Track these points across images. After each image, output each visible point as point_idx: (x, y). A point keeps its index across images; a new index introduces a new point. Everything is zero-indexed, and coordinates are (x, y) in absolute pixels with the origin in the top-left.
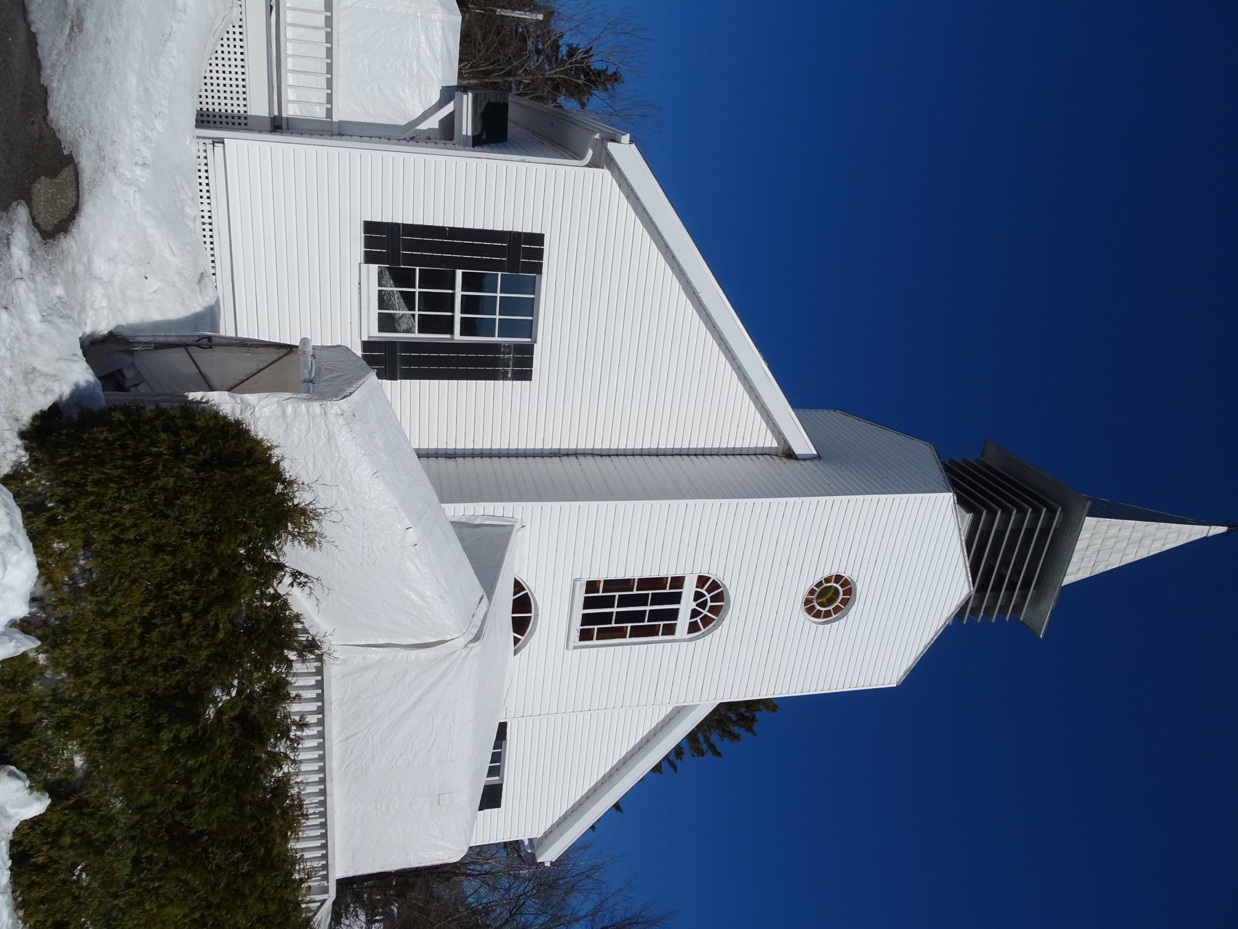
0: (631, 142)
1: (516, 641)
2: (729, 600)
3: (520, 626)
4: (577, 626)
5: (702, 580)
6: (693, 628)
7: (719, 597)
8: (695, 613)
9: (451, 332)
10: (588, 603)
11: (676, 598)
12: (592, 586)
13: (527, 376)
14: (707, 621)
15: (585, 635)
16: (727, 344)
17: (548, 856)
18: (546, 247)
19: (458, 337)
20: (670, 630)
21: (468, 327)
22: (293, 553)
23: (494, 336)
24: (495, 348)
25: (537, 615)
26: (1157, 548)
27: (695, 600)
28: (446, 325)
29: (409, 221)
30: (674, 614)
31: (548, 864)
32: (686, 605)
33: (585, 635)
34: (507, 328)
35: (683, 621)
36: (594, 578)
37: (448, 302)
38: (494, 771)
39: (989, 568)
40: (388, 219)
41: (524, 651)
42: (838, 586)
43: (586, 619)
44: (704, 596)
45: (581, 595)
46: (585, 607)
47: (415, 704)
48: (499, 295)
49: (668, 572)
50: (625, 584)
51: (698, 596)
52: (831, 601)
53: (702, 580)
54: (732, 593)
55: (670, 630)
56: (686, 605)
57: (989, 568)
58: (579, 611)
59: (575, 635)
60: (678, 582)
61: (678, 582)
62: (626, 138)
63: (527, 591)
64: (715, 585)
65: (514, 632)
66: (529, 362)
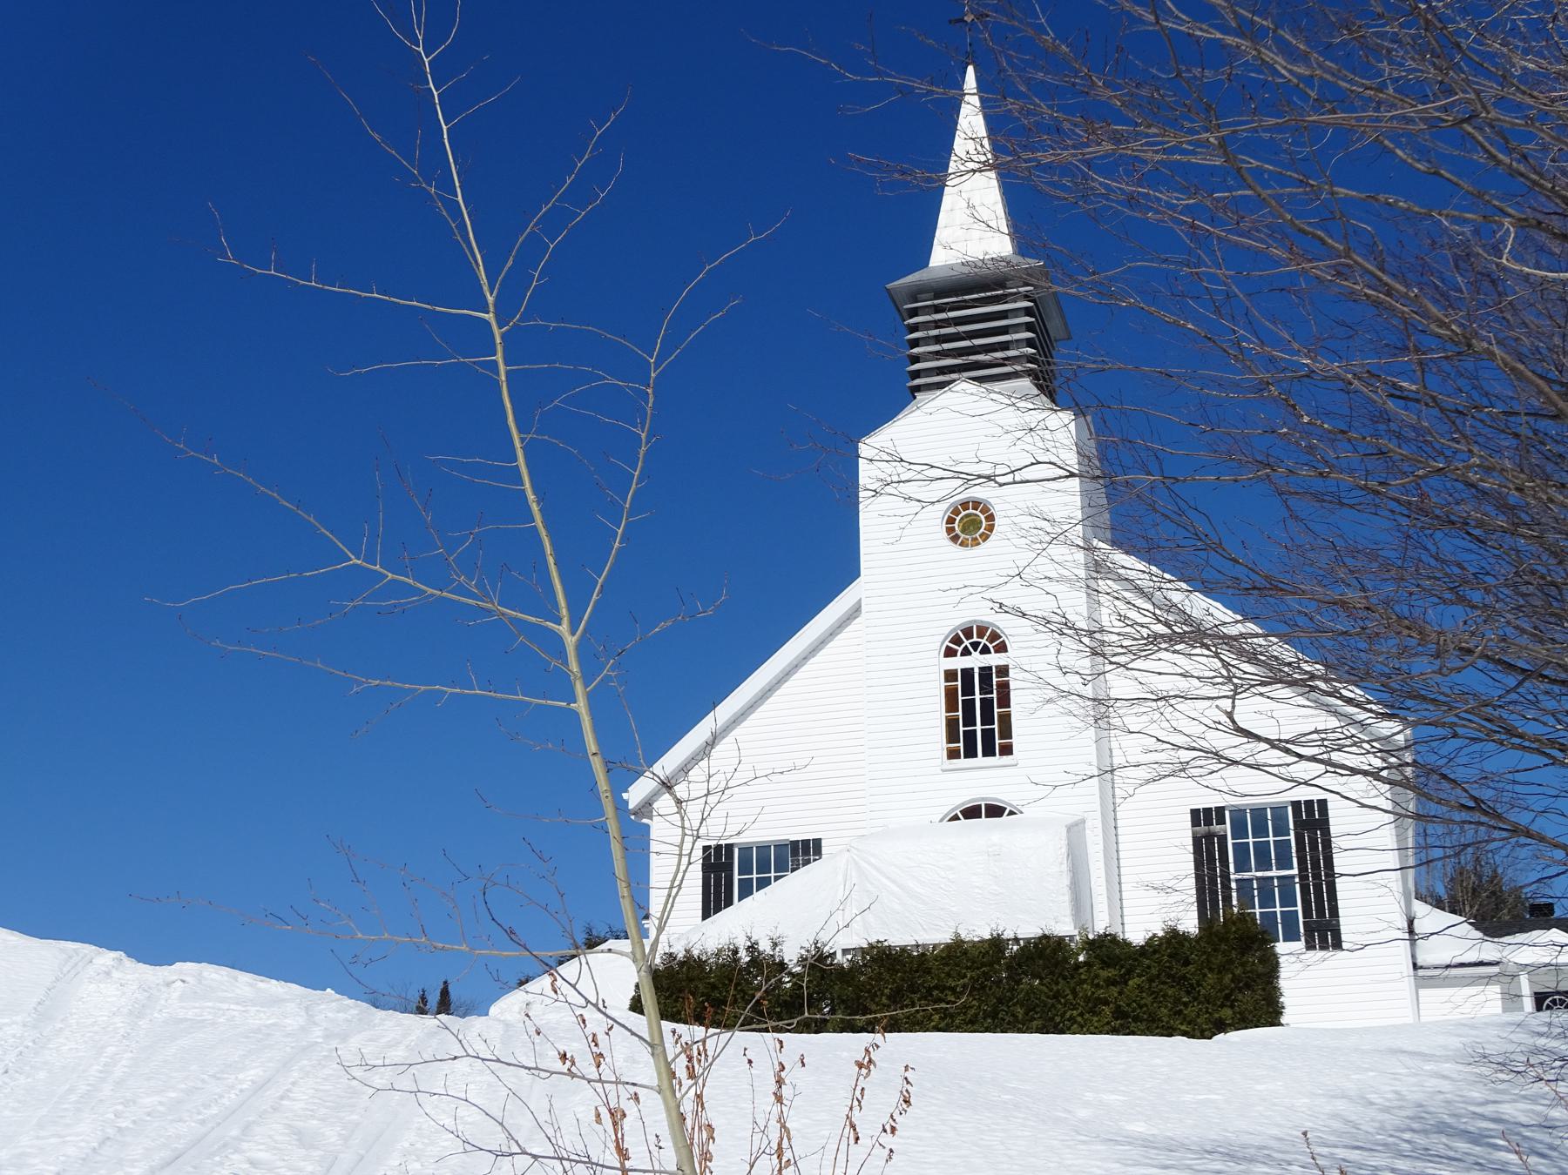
0: (626, 791)
1: (1012, 813)
2: (970, 622)
3: (995, 811)
4: (997, 760)
5: (950, 653)
6: (1002, 648)
7: (968, 632)
8: (985, 651)
9: (1293, 877)
10: (971, 752)
11: (967, 674)
12: (953, 754)
14: (995, 636)
15: (1007, 750)
16: (788, 669)
18: (1201, 807)
20: (1003, 671)
23: (1296, 911)
25: (983, 799)
27: (970, 654)
30: (986, 672)
32: (976, 661)
33: (1007, 750)
34: (1281, 829)
35: (994, 660)
36: (945, 753)
38: (956, 818)
39: (941, 371)
42: (958, 519)
43: (989, 751)
44: (980, 643)
45: (963, 762)
47: (894, 882)
48: (755, 876)
50: (952, 725)
51: (966, 652)
52: (978, 524)
54: (958, 622)
55: (1003, 671)
56: (976, 661)
57: (941, 371)
58: (980, 760)
59: (1006, 759)
60: (950, 675)
61: (950, 675)
62: (625, 796)
64: (957, 640)
65: (1001, 816)
66: (806, 843)
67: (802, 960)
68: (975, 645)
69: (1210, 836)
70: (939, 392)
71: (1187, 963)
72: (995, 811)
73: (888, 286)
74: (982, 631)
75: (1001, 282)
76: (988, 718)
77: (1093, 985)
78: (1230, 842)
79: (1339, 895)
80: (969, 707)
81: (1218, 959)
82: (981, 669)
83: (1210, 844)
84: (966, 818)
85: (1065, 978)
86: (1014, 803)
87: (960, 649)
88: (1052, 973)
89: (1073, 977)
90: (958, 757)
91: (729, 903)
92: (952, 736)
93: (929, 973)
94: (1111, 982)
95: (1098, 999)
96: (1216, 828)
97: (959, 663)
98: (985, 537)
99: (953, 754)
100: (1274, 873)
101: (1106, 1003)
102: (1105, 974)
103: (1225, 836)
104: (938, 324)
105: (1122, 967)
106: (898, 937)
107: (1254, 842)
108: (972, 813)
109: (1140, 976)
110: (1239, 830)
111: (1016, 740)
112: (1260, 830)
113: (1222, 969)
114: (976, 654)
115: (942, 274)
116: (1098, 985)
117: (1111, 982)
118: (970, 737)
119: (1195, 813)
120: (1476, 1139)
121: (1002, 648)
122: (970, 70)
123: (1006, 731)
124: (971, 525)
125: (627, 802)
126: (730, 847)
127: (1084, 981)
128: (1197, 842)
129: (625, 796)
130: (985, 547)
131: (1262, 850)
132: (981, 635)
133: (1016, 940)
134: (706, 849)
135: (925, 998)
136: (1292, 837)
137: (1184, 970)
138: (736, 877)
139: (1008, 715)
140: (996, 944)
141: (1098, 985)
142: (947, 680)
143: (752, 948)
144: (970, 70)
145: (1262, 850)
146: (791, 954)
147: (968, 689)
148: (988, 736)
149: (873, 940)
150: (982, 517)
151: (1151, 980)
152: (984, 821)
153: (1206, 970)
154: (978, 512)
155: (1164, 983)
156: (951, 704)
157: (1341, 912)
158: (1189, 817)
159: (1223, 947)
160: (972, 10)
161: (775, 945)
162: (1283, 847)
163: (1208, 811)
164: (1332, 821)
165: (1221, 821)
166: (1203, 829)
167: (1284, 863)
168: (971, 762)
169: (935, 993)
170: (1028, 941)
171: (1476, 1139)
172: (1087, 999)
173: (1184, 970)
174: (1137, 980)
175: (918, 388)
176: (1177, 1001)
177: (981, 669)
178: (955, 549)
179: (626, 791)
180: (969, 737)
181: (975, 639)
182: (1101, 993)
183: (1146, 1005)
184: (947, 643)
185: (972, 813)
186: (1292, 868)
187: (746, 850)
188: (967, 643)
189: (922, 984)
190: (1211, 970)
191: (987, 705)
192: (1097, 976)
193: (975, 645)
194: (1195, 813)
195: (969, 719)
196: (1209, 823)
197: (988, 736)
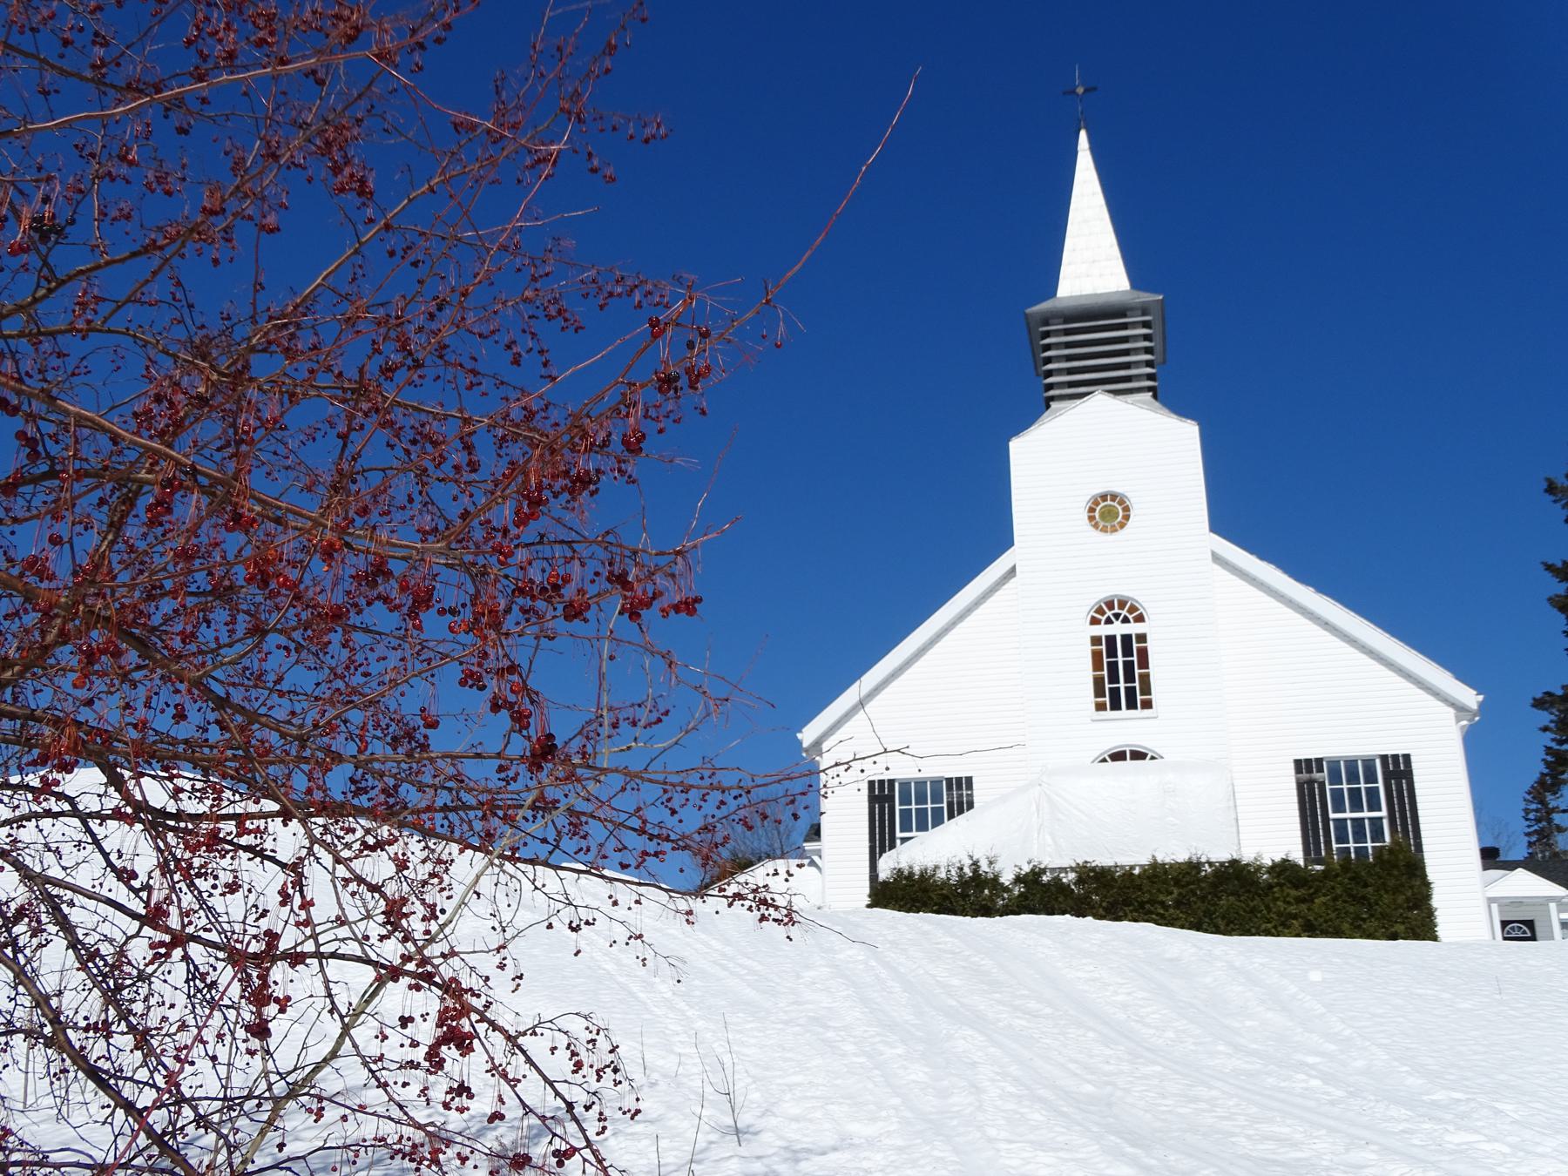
3: (1138, 755)
4: (1139, 712)
5: (1094, 621)
6: (1140, 619)
7: (1110, 605)
8: (1126, 620)
9: (1381, 818)
10: (1116, 706)
11: (1111, 640)
12: (1100, 707)
13: (1303, 766)
14: (1133, 609)
15: (1147, 705)
17: (1470, 698)
19: (1384, 813)
20: (1142, 638)
21: (1373, 805)
22: (942, 875)
26: (1099, 200)
28: (1376, 823)
30: (1127, 639)
31: (1481, 698)
32: (1118, 629)
33: (1147, 705)
34: (1370, 777)
35: (1133, 629)
36: (1093, 706)
37: (1358, 823)
38: (1104, 760)
43: (1132, 705)
45: (1109, 714)
46: (1136, 708)
49: (1088, 649)
50: (1098, 683)
51: (1109, 621)
54: (1093, 602)
55: (1142, 638)
58: (1124, 712)
59: (1147, 712)
60: (1096, 640)
61: (1096, 640)
62: (799, 736)
63: (1128, 750)
64: (1100, 611)
67: (1018, 880)
68: (1117, 616)
69: (1311, 782)
70: (1078, 402)
71: (1366, 885)
72: (1138, 755)
73: (1029, 311)
74: (1122, 604)
76: (1129, 677)
77: (1285, 902)
78: (1328, 787)
79: (1423, 834)
80: (1113, 667)
81: (1392, 882)
85: (1259, 896)
86: (1157, 750)
87: (1103, 619)
88: (1249, 891)
89: (1267, 895)
90: (1105, 709)
91: (942, 822)
92: (1099, 691)
93: (1140, 889)
94: (1299, 900)
95: (1290, 914)
96: (1316, 775)
97: (1103, 630)
98: (1122, 526)
99: (1100, 707)
100: (1348, 815)
101: (1295, 917)
102: (1294, 893)
103: (1323, 783)
104: (1068, 345)
105: (1310, 887)
106: (1103, 858)
107: (1349, 789)
108: (1118, 756)
109: (1325, 895)
110: (1335, 777)
111: (1155, 696)
112: (921, 799)
113: (1396, 891)
114: (1117, 624)
115: (1072, 303)
116: (1289, 903)
117: (1299, 900)
118: (1115, 693)
119: (1298, 763)
122: (1083, 135)
124: (1109, 514)
125: (800, 743)
126: (891, 782)
127: (1277, 899)
128: (1300, 786)
129: (799, 736)
130: (1121, 534)
131: (1354, 794)
132: (1103, 613)
133: (1211, 864)
135: (1136, 911)
137: (1363, 891)
138: (898, 808)
139: (1147, 675)
140: (1193, 867)
141: (1289, 903)
142: (1093, 644)
143: (975, 864)
144: (1083, 135)
145: (1354, 794)
146: (917, 870)
147: (1112, 652)
148: (1131, 693)
149: (1080, 862)
150: (1120, 508)
151: (1335, 899)
152: (1129, 764)
153: (1382, 892)
154: (1115, 504)
155: (1345, 902)
156: (1097, 665)
157: (1425, 848)
158: (1292, 766)
159: (1396, 873)
160: (1082, 84)
161: (991, 863)
162: (1372, 794)
163: (1308, 761)
164: (1415, 772)
165: (1320, 770)
166: (1305, 776)
168: (1116, 714)
169: (1147, 906)
170: (1222, 864)
172: (1280, 914)
173: (1363, 891)
174: (1323, 899)
175: (1052, 398)
176: (1358, 917)
179: (800, 731)
180: (1115, 693)
181: (1116, 610)
182: (1293, 909)
183: (1331, 920)
184: (1092, 613)
185: (1118, 756)
186: (1380, 809)
187: (905, 785)
188: (1109, 613)
189: (1135, 899)
190: (1387, 892)
191: (1129, 667)
192: (1288, 895)
193: (1117, 616)
194: (1298, 763)
195: (1114, 678)
196: (1310, 771)
197: (1131, 693)
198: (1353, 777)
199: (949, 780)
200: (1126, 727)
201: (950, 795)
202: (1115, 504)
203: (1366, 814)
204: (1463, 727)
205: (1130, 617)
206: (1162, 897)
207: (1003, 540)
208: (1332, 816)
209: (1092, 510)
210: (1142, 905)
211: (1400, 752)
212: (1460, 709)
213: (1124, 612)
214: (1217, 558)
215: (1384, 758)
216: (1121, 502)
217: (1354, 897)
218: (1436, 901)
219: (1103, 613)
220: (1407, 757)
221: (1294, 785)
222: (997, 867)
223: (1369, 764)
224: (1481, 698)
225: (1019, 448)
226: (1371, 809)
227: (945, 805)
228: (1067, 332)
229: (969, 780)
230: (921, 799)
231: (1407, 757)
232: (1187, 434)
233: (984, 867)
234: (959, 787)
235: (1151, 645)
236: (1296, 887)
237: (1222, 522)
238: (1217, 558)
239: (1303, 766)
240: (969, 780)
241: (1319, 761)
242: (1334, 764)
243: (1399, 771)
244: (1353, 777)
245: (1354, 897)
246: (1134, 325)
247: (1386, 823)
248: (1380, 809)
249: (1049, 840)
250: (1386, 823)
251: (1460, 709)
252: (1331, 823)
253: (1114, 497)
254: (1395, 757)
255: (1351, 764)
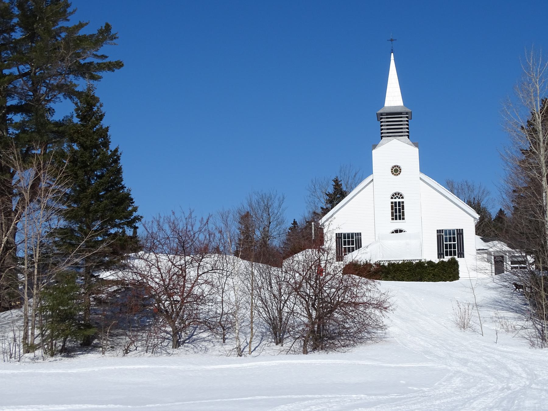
1: (404, 232)
3: (401, 231)
4: (401, 221)
5: (392, 198)
6: (403, 198)
7: (396, 194)
8: (399, 198)
10: (396, 219)
11: (396, 203)
12: (393, 219)
13: (439, 231)
14: (401, 195)
15: (403, 219)
17: (478, 216)
18: (439, 229)
20: (403, 202)
21: (454, 241)
24: (356, 239)
28: (454, 245)
29: (437, 252)
30: (399, 202)
31: (479, 216)
32: (397, 200)
33: (403, 219)
34: (454, 234)
35: (401, 200)
38: (393, 232)
40: (437, 255)
41: (406, 230)
43: (400, 219)
45: (395, 221)
48: (452, 236)
50: (392, 213)
51: (395, 198)
53: (392, 198)
55: (403, 202)
58: (398, 221)
60: (392, 203)
61: (392, 203)
64: (393, 195)
67: (375, 264)
68: (397, 197)
69: (440, 235)
71: (445, 267)
72: (401, 231)
74: (399, 194)
75: (401, 113)
78: (444, 236)
81: (450, 266)
82: (398, 202)
83: (440, 237)
84: (396, 233)
87: (394, 197)
91: (354, 251)
94: (432, 270)
96: (441, 234)
97: (394, 200)
99: (393, 219)
101: (431, 273)
102: (431, 268)
108: (396, 231)
110: (446, 234)
111: (390, 205)
113: (451, 268)
114: (397, 199)
117: (432, 270)
119: (437, 230)
120: (500, 303)
121: (403, 198)
122: (392, 54)
123: (403, 215)
126: (341, 234)
132: (398, 195)
134: (336, 234)
136: (456, 236)
137: (445, 268)
138: (343, 240)
143: (366, 262)
144: (392, 54)
151: (439, 270)
157: (464, 251)
162: (454, 238)
165: (442, 232)
166: (439, 234)
167: (454, 241)
171: (500, 303)
172: (428, 273)
173: (445, 268)
176: (443, 273)
177: (398, 202)
178: (393, 176)
181: (397, 195)
182: (430, 272)
185: (396, 231)
186: (455, 242)
187: (345, 234)
188: (395, 196)
191: (399, 209)
194: (437, 230)
196: (440, 233)
198: (450, 234)
199: (356, 233)
200: (398, 224)
201: (356, 237)
202: (398, 168)
203: (452, 243)
204: (475, 223)
205: (400, 197)
206: (405, 269)
207: (370, 172)
208: (444, 243)
209: (392, 169)
210: (401, 271)
211: (461, 229)
212: (475, 218)
213: (399, 196)
214: (421, 179)
215: (457, 230)
216: (399, 168)
217: (443, 269)
218: (460, 269)
219: (394, 196)
220: (462, 230)
221: (436, 236)
222: (391, 312)
223: (454, 231)
224: (479, 216)
225: (375, 153)
226: (453, 242)
227: (354, 239)
228: (387, 118)
229: (360, 233)
230: (349, 238)
231: (462, 230)
232: (416, 150)
233: (368, 261)
234: (358, 235)
235: (405, 204)
236: (432, 267)
237: (423, 169)
238: (421, 179)
239: (439, 231)
240: (360, 233)
241: (442, 230)
242: (446, 231)
243: (460, 233)
244: (450, 234)
245: (443, 269)
246: (404, 117)
247: (456, 244)
248: (455, 242)
249: (381, 254)
250: (456, 244)
251: (475, 218)
252: (444, 245)
253: (397, 166)
254: (460, 229)
255: (450, 231)
